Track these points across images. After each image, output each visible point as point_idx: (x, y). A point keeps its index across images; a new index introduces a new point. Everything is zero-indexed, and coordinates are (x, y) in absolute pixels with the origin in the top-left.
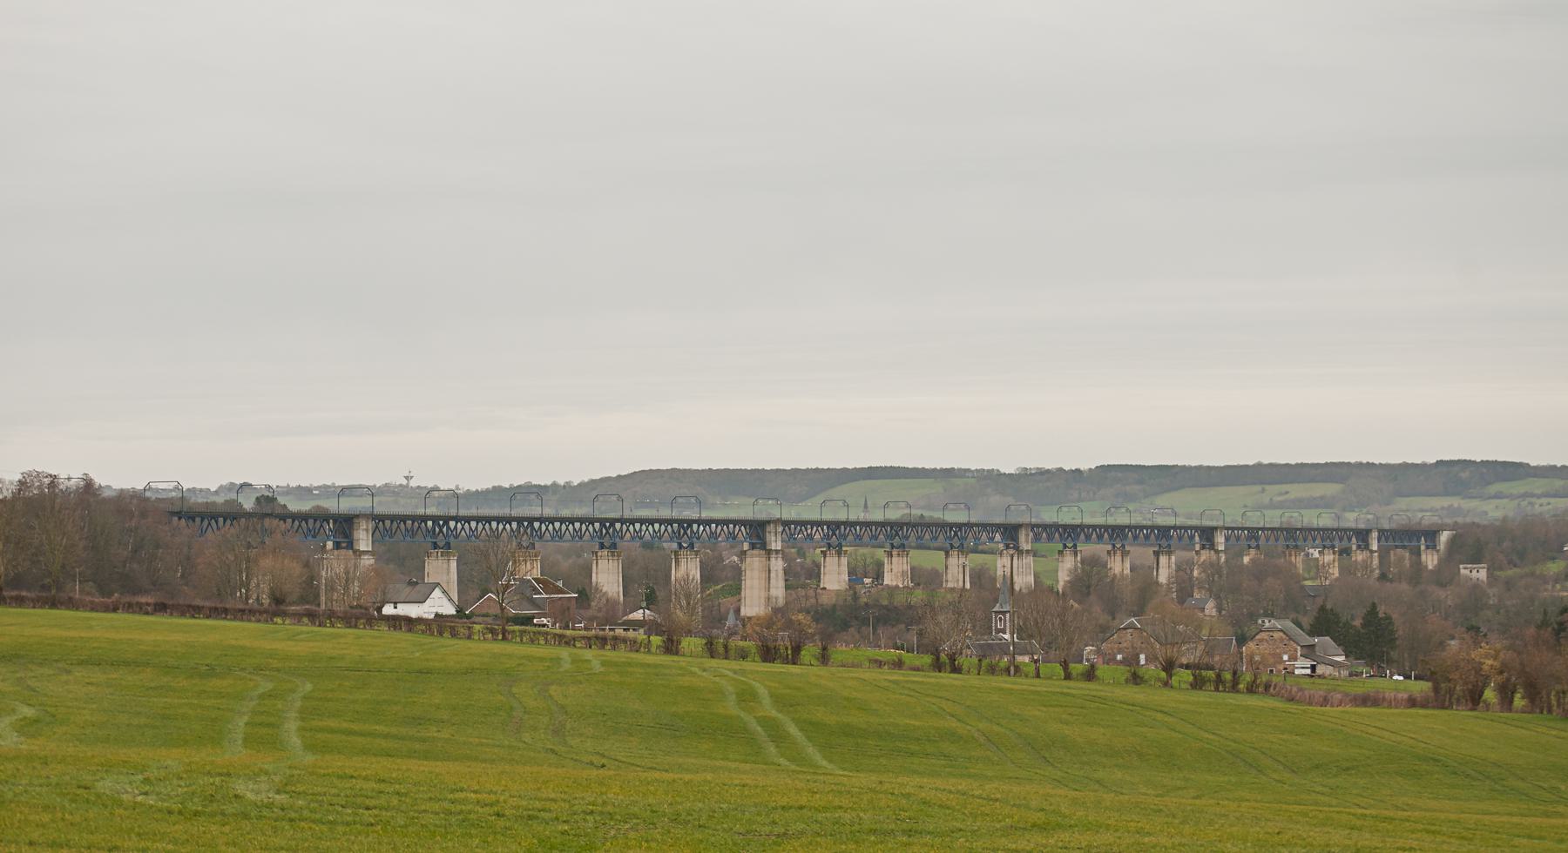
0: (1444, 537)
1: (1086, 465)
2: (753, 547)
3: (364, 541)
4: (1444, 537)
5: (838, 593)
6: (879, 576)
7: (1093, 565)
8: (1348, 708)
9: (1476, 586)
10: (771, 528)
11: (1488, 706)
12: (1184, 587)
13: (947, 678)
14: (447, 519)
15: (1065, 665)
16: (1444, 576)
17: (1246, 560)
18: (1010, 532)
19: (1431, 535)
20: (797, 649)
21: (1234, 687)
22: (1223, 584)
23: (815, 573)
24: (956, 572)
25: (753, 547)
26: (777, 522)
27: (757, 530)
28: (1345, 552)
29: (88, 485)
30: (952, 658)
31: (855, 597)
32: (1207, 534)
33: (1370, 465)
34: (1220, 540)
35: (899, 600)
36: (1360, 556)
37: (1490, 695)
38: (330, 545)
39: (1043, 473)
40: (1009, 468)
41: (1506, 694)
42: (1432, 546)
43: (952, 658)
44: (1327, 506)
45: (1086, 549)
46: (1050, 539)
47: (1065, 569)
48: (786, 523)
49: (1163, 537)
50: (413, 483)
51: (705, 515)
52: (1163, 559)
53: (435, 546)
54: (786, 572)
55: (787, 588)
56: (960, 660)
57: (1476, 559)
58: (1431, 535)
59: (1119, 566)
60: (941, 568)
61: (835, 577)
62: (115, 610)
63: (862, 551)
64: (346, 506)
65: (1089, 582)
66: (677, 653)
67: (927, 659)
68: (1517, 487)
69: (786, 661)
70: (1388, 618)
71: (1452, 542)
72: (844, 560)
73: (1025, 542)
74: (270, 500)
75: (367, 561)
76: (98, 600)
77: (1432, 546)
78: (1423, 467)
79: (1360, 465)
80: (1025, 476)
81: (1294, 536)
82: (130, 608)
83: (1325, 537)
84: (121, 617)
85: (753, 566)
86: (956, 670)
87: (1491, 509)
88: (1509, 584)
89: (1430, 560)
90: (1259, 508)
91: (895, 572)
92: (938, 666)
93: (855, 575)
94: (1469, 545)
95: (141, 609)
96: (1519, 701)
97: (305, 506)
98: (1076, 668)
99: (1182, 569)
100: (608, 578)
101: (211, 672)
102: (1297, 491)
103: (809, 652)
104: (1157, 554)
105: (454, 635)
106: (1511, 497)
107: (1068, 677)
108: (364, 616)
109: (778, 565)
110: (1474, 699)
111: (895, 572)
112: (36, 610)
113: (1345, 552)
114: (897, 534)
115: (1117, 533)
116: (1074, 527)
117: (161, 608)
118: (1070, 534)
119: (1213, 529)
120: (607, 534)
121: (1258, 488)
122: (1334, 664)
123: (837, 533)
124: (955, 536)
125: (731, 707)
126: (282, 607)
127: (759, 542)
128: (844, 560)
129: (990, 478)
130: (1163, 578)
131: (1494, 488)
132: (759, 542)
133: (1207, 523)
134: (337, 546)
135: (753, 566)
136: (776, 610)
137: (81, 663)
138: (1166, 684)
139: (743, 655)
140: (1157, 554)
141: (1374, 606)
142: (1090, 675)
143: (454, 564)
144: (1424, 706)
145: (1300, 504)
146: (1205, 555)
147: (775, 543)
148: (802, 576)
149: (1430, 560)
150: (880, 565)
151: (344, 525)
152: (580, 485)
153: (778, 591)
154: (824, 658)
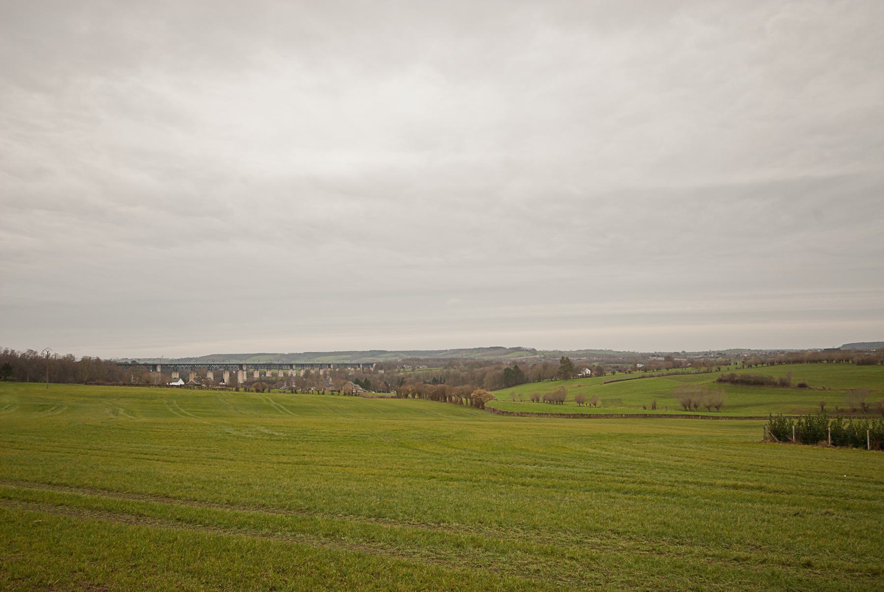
0: (374, 365)
1: (302, 352)
2: (240, 369)
3: (159, 369)
4: (374, 365)
5: (257, 378)
6: (265, 375)
7: (307, 372)
8: (378, 399)
9: (382, 374)
10: (244, 365)
11: (409, 398)
12: (325, 375)
13: (294, 395)
14: (194, 365)
15: (318, 391)
16: (376, 372)
17: (337, 370)
18: (291, 365)
19: (372, 364)
20: (263, 390)
21: (352, 395)
22: (333, 374)
23: (253, 374)
24: (281, 374)
25: (240, 369)
26: (245, 364)
27: (241, 366)
28: (355, 368)
29: (98, 359)
30: (295, 391)
31: (261, 379)
32: (329, 365)
33: (357, 352)
34: (332, 366)
35: (270, 379)
36: (358, 369)
37: (410, 395)
38: (151, 371)
39: (293, 354)
40: (286, 353)
41: (413, 397)
42: (372, 367)
43: (295, 391)
44: (349, 359)
45: (307, 368)
46: (299, 366)
47: (302, 373)
48: (247, 364)
49: (321, 366)
50: (163, 358)
51: (215, 363)
52: (321, 370)
53: (174, 370)
54: (247, 374)
55: (247, 377)
56: (297, 391)
57: (381, 369)
58: (372, 364)
59: (312, 372)
60: (277, 373)
61: (256, 375)
62: (113, 385)
63: (262, 370)
64: (155, 362)
65: (307, 374)
66: (238, 391)
67: (290, 391)
68: (385, 355)
69: (261, 392)
70: (369, 381)
71: (376, 366)
72: (258, 372)
73: (294, 367)
74: (135, 362)
75: (160, 374)
76: (642, 393)
77: (372, 367)
78: (367, 352)
79: (355, 352)
80: (289, 355)
81: (346, 365)
82: (117, 385)
83: (352, 365)
84: (115, 387)
85: (240, 372)
86: (296, 393)
87: (381, 360)
88: (389, 374)
89: (372, 369)
90: (336, 360)
91: (268, 374)
92: (292, 392)
93: (272, 374)
94: (380, 366)
95: (120, 385)
96: (416, 397)
97: (143, 363)
98: (321, 392)
99: (325, 372)
100: (210, 375)
101: (151, 399)
102: (343, 357)
103: (266, 390)
104: (320, 369)
105: (191, 389)
106: (384, 357)
107: (319, 394)
108: (162, 385)
109: (245, 373)
110: (406, 396)
111: (268, 374)
112: (42, 383)
113: (355, 368)
114: (269, 366)
115: (312, 365)
116: (281, 364)
117: (124, 385)
118: (303, 365)
119: (331, 364)
120: (210, 367)
121: (335, 356)
122: (361, 390)
123: (256, 366)
124: (280, 367)
125: (265, 403)
126: (149, 384)
127: (241, 368)
128: (258, 372)
129: (283, 355)
130: (321, 373)
131: (381, 355)
132: (241, 368)
133: (329, 363)
134: (153, 370)
135: (240, 372)
136: (245, 382)
137: (121, 397)
138: (339, 395)
139: (252, 391)
140: (320, 369)
141: (366, 378)
142: (323, 393)
143: (178, 374)
144: (395, 398)
145: (343, 359)
146: (329, 369)
147: (245, 369)
148: (250, 375)
149: (372, 369)
150: (265, 373)
151: (154, 366)
152: (509, 349)
153: (245, 378)
154: (269, 392)
